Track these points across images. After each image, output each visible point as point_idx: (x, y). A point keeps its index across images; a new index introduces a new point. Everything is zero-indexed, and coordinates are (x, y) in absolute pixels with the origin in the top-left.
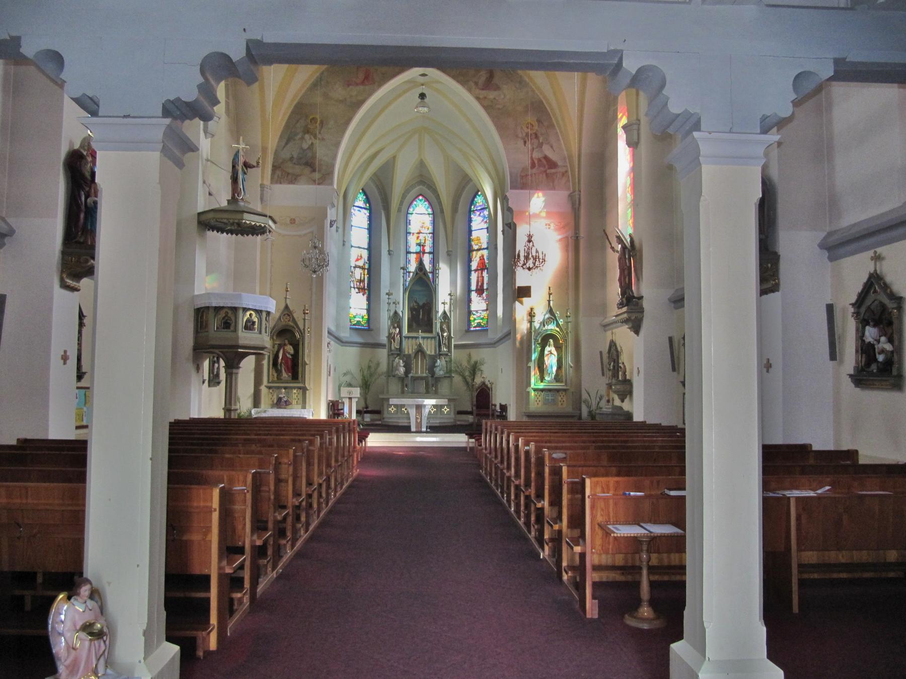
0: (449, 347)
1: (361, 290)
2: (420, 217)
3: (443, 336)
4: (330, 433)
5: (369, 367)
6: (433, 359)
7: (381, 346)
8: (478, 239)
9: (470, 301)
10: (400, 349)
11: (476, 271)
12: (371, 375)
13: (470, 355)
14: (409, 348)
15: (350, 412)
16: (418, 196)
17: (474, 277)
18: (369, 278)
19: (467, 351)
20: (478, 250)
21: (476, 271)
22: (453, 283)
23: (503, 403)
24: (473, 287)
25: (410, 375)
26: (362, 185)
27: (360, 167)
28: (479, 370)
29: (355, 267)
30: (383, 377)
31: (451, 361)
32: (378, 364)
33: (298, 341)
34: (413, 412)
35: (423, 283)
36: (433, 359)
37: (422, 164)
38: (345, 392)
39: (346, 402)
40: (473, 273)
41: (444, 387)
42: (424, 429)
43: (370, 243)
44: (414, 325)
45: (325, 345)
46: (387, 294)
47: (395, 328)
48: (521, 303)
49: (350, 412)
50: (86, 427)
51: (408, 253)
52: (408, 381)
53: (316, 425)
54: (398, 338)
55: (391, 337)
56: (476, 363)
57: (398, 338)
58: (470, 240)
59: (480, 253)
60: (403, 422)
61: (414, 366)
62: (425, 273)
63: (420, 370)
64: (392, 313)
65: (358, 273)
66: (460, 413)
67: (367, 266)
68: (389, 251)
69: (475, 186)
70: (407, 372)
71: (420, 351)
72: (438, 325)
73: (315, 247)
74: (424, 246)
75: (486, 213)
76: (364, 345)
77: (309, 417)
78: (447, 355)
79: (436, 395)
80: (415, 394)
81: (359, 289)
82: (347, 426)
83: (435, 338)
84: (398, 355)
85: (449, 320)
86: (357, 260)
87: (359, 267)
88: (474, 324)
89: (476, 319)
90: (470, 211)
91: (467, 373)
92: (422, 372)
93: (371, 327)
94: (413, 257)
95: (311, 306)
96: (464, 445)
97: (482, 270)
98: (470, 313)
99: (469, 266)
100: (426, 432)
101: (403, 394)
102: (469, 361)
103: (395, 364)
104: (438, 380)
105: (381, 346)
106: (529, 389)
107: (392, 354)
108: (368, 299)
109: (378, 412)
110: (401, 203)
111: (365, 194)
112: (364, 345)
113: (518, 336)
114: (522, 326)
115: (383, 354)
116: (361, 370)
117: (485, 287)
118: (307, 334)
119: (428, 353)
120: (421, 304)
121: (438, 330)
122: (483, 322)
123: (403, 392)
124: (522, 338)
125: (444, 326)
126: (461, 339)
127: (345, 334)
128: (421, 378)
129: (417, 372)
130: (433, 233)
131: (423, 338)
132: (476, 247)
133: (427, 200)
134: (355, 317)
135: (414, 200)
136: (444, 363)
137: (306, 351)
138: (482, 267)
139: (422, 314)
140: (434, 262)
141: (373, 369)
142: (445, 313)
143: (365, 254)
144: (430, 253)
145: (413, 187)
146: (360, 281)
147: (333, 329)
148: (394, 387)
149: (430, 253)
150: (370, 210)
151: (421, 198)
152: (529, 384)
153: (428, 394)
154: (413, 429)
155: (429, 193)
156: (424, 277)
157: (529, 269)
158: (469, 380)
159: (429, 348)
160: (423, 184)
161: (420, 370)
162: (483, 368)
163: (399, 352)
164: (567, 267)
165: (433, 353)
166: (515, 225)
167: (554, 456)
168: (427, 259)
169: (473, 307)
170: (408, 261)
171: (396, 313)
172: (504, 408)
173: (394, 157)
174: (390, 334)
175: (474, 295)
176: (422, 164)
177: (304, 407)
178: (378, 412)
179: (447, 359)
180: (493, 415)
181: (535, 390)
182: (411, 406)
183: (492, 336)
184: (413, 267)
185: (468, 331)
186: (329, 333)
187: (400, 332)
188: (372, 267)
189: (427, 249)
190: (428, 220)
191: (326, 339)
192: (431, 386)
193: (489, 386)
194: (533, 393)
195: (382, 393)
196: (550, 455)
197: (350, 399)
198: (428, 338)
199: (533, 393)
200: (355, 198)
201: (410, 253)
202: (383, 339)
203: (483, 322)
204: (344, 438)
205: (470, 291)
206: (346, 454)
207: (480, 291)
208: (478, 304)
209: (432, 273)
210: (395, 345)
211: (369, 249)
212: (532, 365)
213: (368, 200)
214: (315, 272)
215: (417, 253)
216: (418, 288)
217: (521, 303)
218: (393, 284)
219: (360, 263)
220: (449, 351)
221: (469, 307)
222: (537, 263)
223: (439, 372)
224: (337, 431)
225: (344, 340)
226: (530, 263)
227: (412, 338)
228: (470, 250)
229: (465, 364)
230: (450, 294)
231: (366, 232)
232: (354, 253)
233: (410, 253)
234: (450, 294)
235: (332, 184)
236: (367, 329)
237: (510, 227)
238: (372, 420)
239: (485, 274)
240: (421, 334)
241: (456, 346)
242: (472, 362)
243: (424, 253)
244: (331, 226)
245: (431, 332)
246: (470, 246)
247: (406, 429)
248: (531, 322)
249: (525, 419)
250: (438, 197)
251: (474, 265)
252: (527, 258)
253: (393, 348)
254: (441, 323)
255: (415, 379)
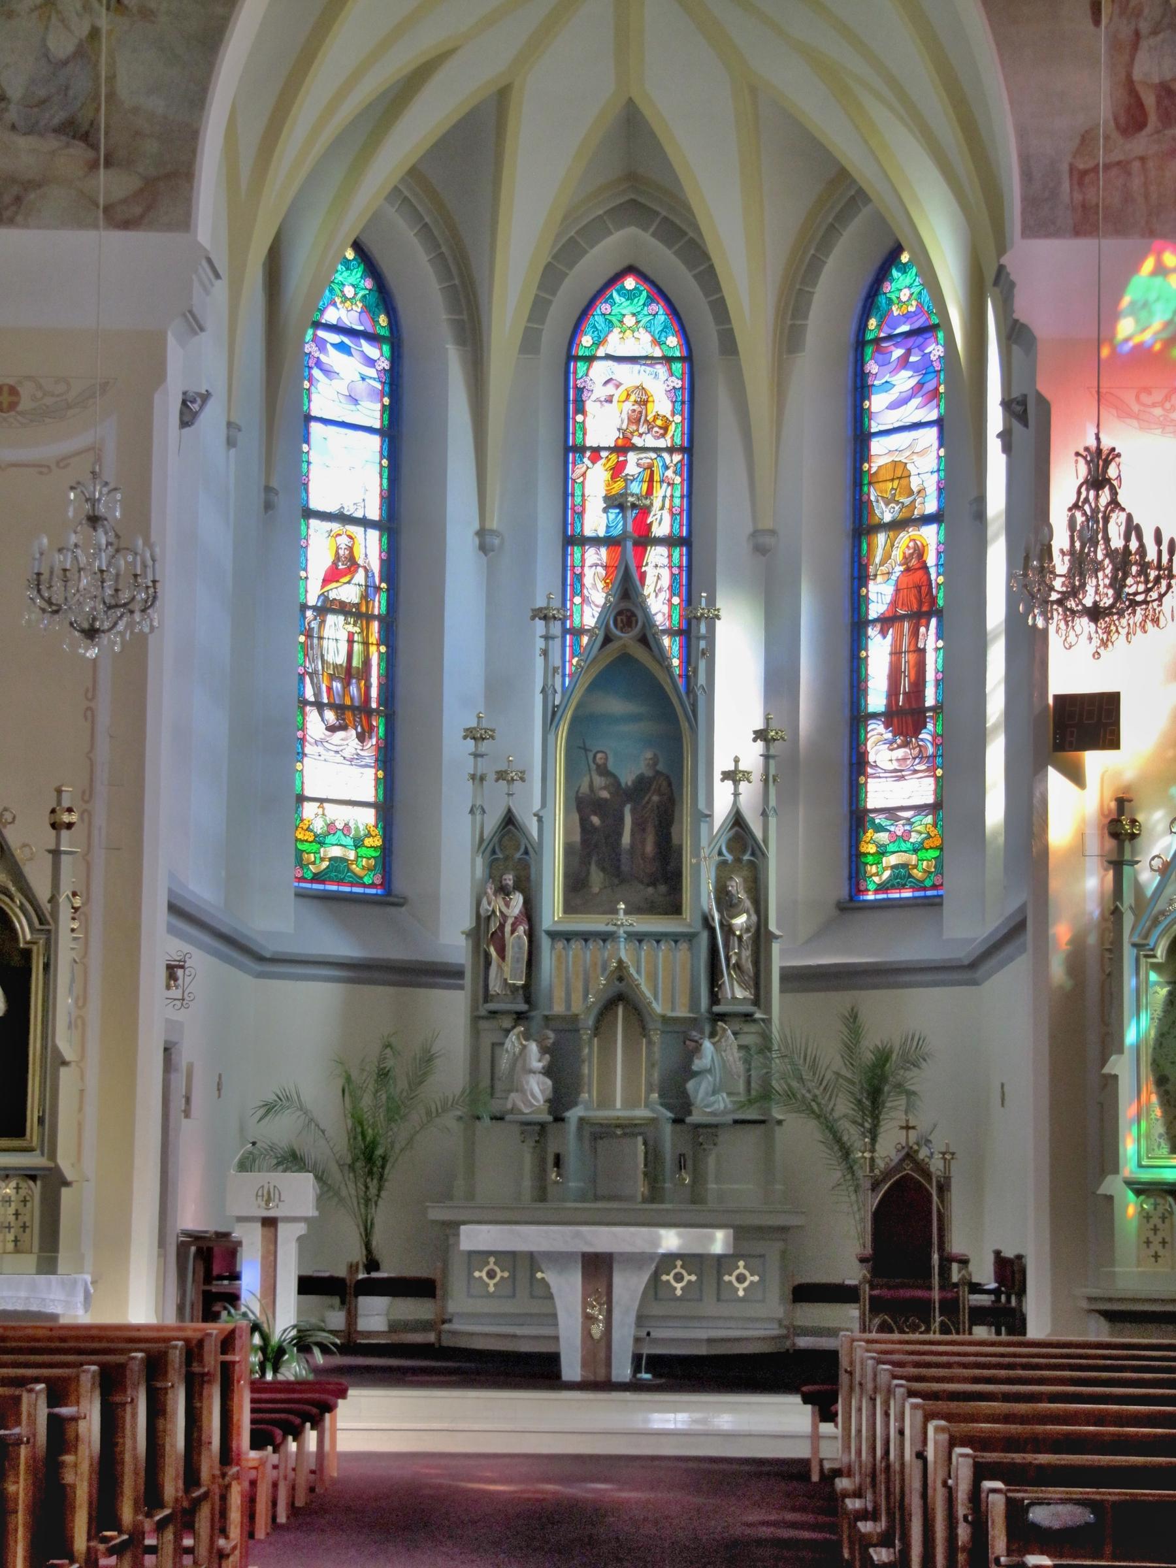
0: (758, 983)
1: (352, 715)
2: (628, 372)
3: (728, 930)
4: (59, 1393)
5: (383, 1075)
6: (684, 1036)
7: (438, 974)
8: (900, 473)
9: (858, 764)
10: (528, 992)
11: (886, 622)
12: (394, 1112)
13: (852, 1020)
14: (568, 983)
15: (271, 1299)
16: (615, 279)
17: (879, 652)
18: (390, 660)
19: (840, 1000)
20: (898, 525)
21: (886, 622)
22: (779, 681)
23: (1009, 1253)
24: (876, 700)
25: (573, 1115)
26: (352, 223)
27: (338, 142)
28: (899, 1087)
29: (327, 607)
30: (449, 1120)
31: (766, 1046)
32: (427, 1060)
33: (27, 954)
34: (567, 1289)
35: (642, 684)
36: (684, 1036)
37: (632, 129)
38: (243, 1198)
39: (251, 1241)
40: (873, 632)
41: (733, 1168)
42: (622, 1371)
43: (392, 498)
44: (597, 878)
45: (152, 975)
46: (470, 734)
47: (503, 891)
48: (1076, 776)
49: (271, 1299)
50: (655, 1194)
51: (573, 540)
52: (569, 1142)
53: (116, 1360)
54: (516, 940)
55: (486, 935)
56: (883, 1057)
57: (516, 940)
58: (858, 479)
59: (904, 540)
60: (525, 1338)
61: (590, 1070)
62: (647, 638)
63: (620, 1088)
64: (492, 822)
65: (336, 636)
66: (804, 1293)
67: (379, 605)
68: (481, 533)
69: (881, 223)
70: (559, 1103)
71: (621, 999)
72: (708, 886)
73: (94, 520)
74: (645, 511)
75: (935, 350)
76: (362, 972)
77: (73, 1311)
78: (748, 1017)
79: (695, 1211)
80: (603, 1201)
81: (339, 709)
82: (176, 1357)
83: (690, 937)
84: (520, 1017)
85: (759, 852)
86: (332, 576)
87: (343, 609)
88: (878, 873)
89: (888, 856)
90: (860, 343)
91: (843, 1107)
92: (630, 1103)
93: (400, 885)
94: (594, 559)
95: (88, 794)
96: (801, 1451)
97: (919, 617)
98: (858, 819)
99: (858, 602)
100: (634, 1386)
101: (541, 1201)
102: (851, 1048)
103: (504, 1063)
104: (703, 1135)
105: (438, 974)
106: (1112, 1185)
107: (486, 1014)
108: (387, 759)
109: (423, 1288)
110: (539, 309)
111: (372, 269)
112: (362, 972)
113: (1062, 932)
114: (1082, 889)
115: (449, 1013)
116: (349, 1089)
117: (930, 701)
118: (65, 922)
119: (658, 1008)
120: (627, 778)
121: (708, 901)
122: (922, 864)
123: (542, 1194)
124: (1078, 943)
125: (737, 886)
126: (824, 931)
127: (278, 921)
128: (629, 1129)
129: (606, 1101)
130: (688, 450)
131: (639, 938)
132: (887, 515)
133: (659, 293)
134: (320, 840)
135: (601, 293)
136: (734, 1056)
137: (64, 1002)
138: (917, 606)
139: (636, 829)
140: (692, 585)
141: (401, 1084)
142: (737, 820)
143: (370, 548)
144: (669, 542)
145: (594, 231)
146: (348, 674)
147: (203, 892)
148: (503, 1161)
149: (669, 542)
150: (395, 341)
151: (630, 283)
152: (1109, 1160)
153: (656, 1204)
154: (571, 1369)
155: (663, 258)
156: (639, 653)
157: (1095, 613)
158: (852, 1135)
159: (665, 982)
160: (640, 210)
161: (620, 1088)
162: (916, 1079)
163: (525, 1007)
164: (694, 729)
165: (682, 1012)
166: (1044, 407)
167: (1039, 1515)
168: (658, 567)
169: (879, 793)
170: (570, 581)
171: (509, 821)
172: (1011, 1272)
173: (501, 98)
174: (482, 921)
175: (877, 735)
176: (632, 129)
177: (48, 1265)
178: (423, 1288)
179: (750, 1040)
180: (950, 1307)
181: (1142, 1189)
182: (559, 1259)
183: (964, 928)
184: (591, 606)
185: (851, 904)
186: (174, 909)
187: (530, 914)
188: (402, 603)
189: (661, 527)
190: (661, 388)
191: (161, 942)
192: (675, 1163)
193: (936, 1166)
194: (1131, 1207)
195: (446, 1196)
196: (1016, 1511)
197: (270, 1223)
198: (658, 938)
199: (1131, 1207)
200: (323, 282)
201: (584, 541)
202: (452, 940)
203: (922, 864)
204: (157, 1410)
205: (858, 718)
206: (172, 1487)
207: (906, 717)
208: (897, 784)
209: (686, 633)
210: (507, 972)
211: (391, 523)
212: (1122, 1067)
213: (383, 296)
214: (91, 633)
215: (609, 541)
216: (615, 705)
217: (1076, 776)
218: (500, 688)
219: (348, 592)
220: (760, 998)
221: (855, 791)
222: (1132, 586)
223: (711, 1099)
224: (111, 1383)
225: (271, 948)
226: (1097, 590)
227: (586, 937)
228: (862, 526)
229: (831, 1058)
230: (760, 735)
231: (374, 442)
232: (321, 546)
233: (584, 541)
234: (760, 735)
235: (185, 223)
236: (387, 887)
237: (1023, 418)
238: (394, 1327)
239: (930, 639)
240: (625, 921)
241: (796, 979)
242: (869, 1057)
243: (644, 539)
244: (188, 417)
245: (675, 909)
246: (860, 508)
247: (535, 1370)
248: (1118, 864)
249: (1099, 1332)
250: (709, 279)
251: (880, 596)
252: (1081, 565)
253: (495, 987)
254: (723, 864)
255: (600, 1134)
